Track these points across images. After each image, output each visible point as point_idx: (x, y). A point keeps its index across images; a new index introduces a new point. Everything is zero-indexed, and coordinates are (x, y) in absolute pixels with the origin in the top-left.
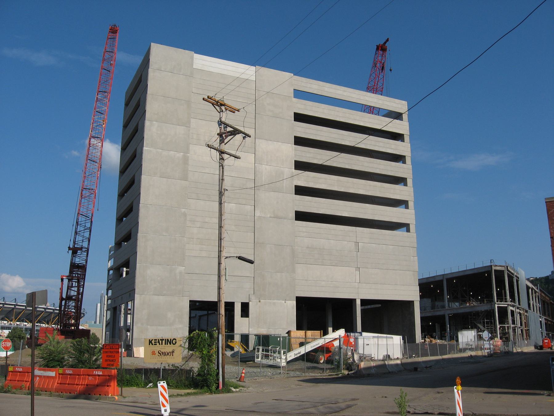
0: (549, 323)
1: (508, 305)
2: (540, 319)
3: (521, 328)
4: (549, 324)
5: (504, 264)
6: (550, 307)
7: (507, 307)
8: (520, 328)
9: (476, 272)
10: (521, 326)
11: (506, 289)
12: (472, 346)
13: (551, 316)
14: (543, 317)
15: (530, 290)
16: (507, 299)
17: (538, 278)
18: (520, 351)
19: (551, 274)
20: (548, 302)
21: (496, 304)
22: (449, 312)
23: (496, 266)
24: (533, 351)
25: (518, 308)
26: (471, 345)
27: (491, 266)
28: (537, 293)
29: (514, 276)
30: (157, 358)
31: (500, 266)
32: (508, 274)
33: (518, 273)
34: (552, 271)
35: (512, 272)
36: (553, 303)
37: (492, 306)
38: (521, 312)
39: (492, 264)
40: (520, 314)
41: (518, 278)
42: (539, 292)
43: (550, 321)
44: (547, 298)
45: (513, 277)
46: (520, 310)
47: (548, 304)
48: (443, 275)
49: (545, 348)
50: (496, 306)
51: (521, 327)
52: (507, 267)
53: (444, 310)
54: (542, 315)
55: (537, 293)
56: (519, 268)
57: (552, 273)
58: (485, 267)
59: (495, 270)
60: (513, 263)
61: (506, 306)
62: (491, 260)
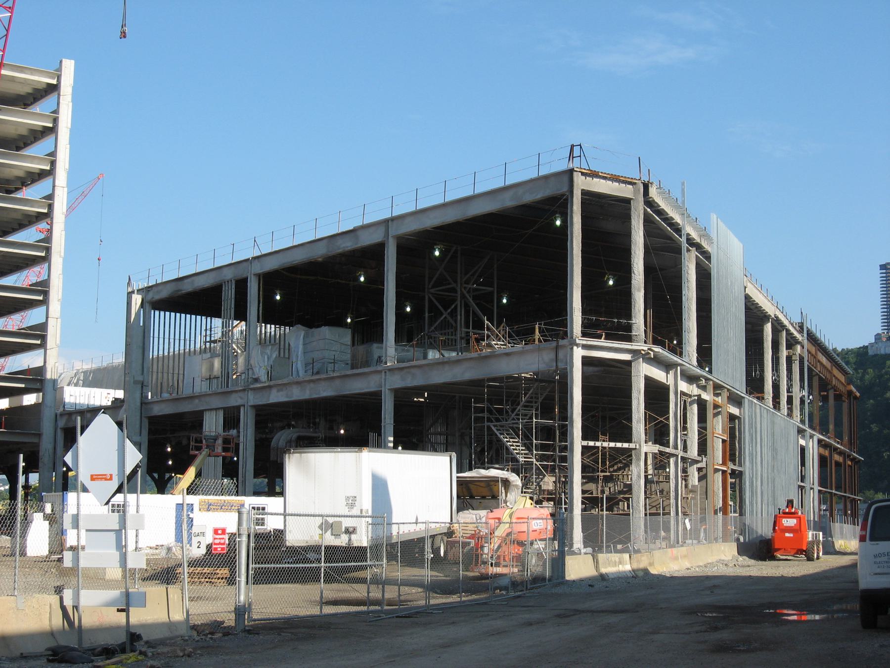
0: (837, 457)
1: (635, 353)
2: (802, 442)
3: (699, 465)
4: (838, 464)
5: (631, 172)
6: (845, 406)
7: (628, 363)
8: (697, 462)
9: (507, 202)
10: (699, 455)
11: (633, 282)
12: (353, 537)
13: (846, 439)
14: (812, 437)
15: (768, 328)
16: (634, 327)
17: (839, 349)
18: (628, 567)
19: (873, 341)
20: (841, 388)
21: (578, 345)
22: (397, 381)
23: (594, 175)
24: (730, 571)
25: (691, 379)
26: (349, 531)
27: (571, 172)
28: (799, 347)
29: (683, 240)
30: (157, 507)
31: (615, 179)
32: (648, 220)
33: (705, 234)
34: (878, 334)
35: (678, 219)
36: (858, 394)
37: (561, 354)
38: (705, 396)
39: (575, 164)
40: (702, 405)
41: (708, 256)
42: (806, 342)
43: (841, 453)
44: (836, 372)
45: (678, 251)
46: (704, 388)
47: (838, 397)
48: (386, 222)
49: (785, 551)
50: (578, 353)
51: (699, 458)
52: (646, 187)
53: (380, 372)
54: (811, 427)
55: (799, 347)
56: (714, 217)
57: (875, 339)
58: (546, 178)
59: (585, 193)
60: (683, 184)
61: (627, 357)
62: (572, 146)
